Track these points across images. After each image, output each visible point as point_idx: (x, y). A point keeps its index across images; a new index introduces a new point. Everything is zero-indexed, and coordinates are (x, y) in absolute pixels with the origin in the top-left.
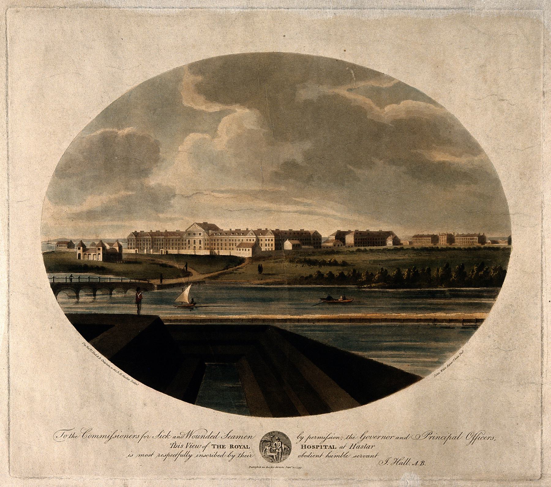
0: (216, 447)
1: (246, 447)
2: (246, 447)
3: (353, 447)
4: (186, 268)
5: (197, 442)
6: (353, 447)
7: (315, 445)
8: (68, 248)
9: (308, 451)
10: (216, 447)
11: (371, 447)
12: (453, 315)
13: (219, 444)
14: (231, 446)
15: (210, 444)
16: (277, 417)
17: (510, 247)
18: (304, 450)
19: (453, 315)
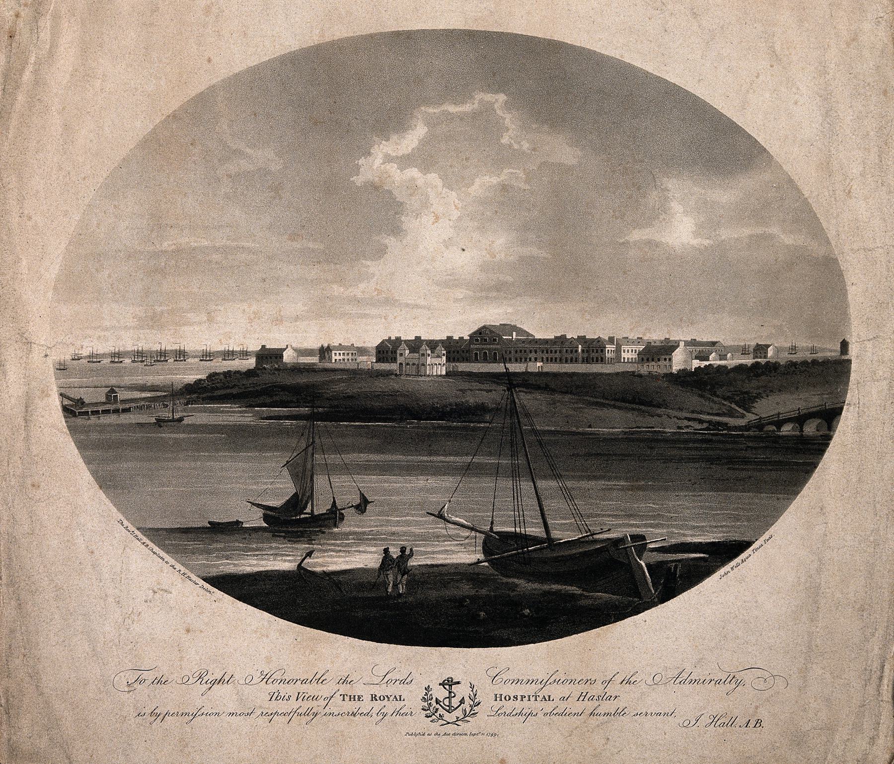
0: (347, 698)
1: (398, 698)
2: (398, 698)
3: (582, 698)
4: (547, 531)
5: (285, 689)
6: (582, 698)
7: (519, 694)
8: (48, 396)
9: (509, 706)
10: (347, 698)
11: (612, 698)
12: (739, 410)
13: (498, 693)
14: (374, 698)
15: (339, 693)
16: (311, 627)
17: (846, 357)
18: (498, 704)
19: (739, 410)
